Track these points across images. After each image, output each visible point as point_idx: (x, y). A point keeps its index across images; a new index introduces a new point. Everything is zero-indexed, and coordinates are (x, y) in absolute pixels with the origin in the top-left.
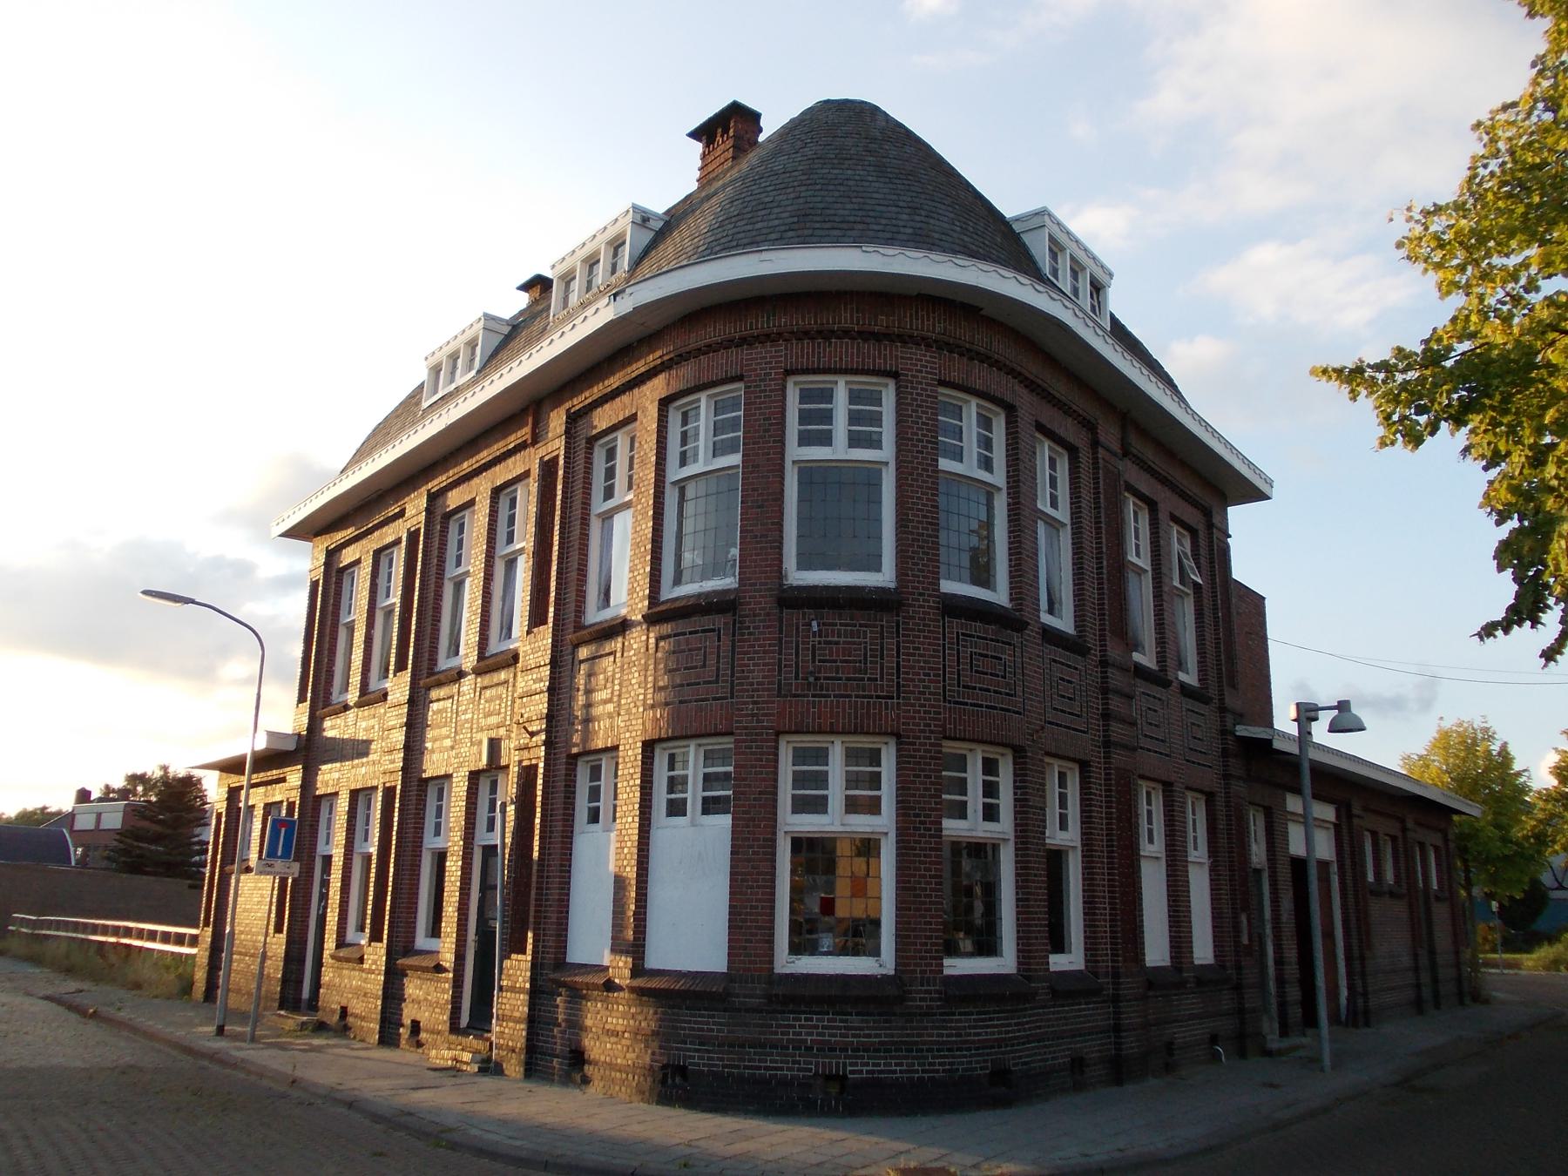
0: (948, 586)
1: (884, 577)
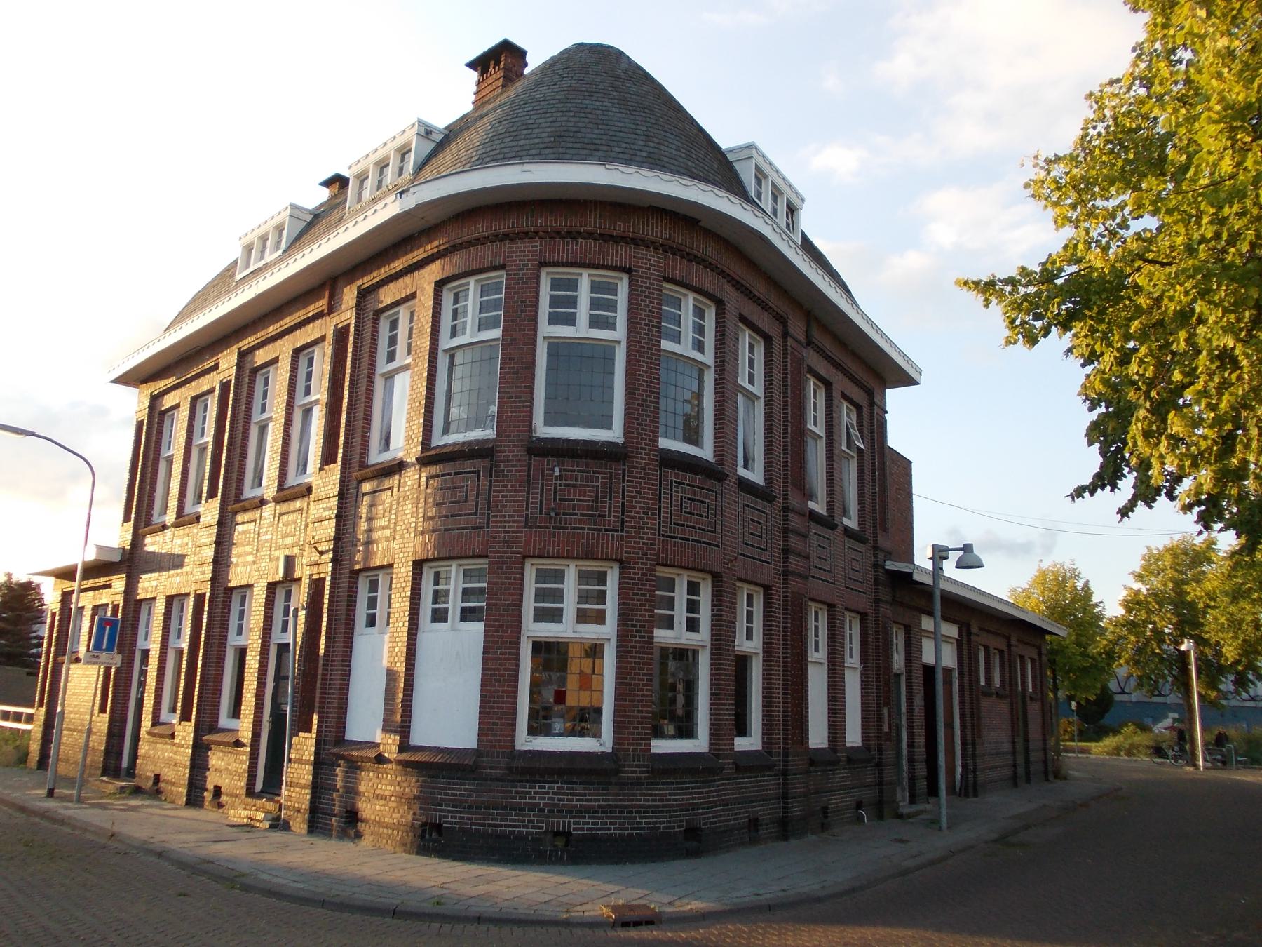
0: (665, 443)
1: (614, 434)
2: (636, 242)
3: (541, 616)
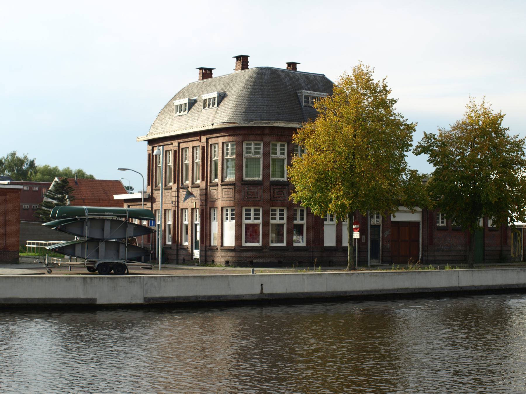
0: (272, 179)
1: (261, 178)
2: (264, 134)
3: (246, 219)
